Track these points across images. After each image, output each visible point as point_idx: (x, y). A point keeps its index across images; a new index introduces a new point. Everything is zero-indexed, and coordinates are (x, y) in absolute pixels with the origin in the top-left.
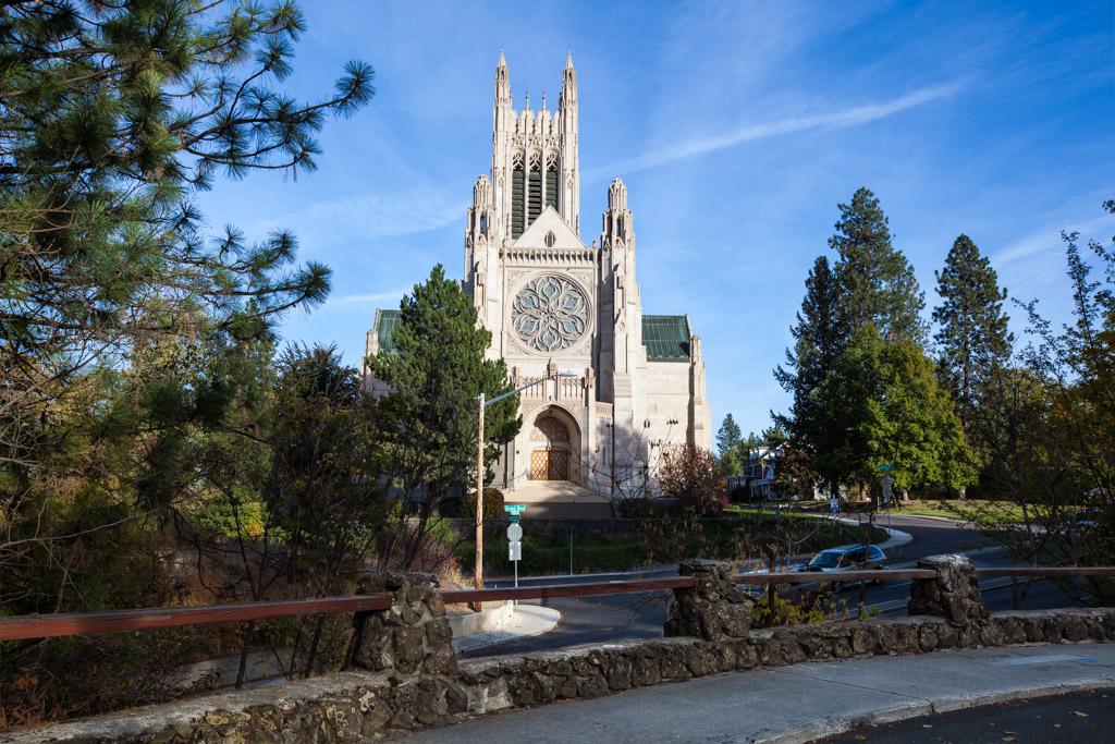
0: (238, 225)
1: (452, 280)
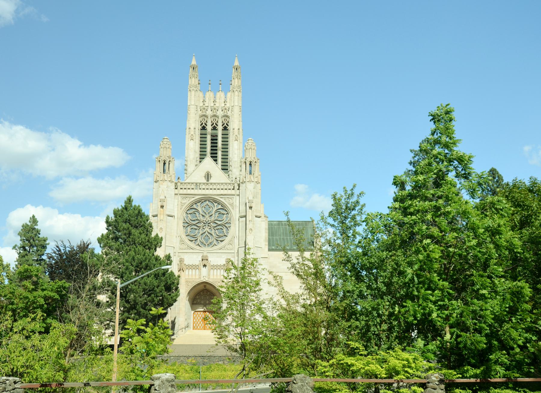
0: (455, 127)
1: (137, 205)
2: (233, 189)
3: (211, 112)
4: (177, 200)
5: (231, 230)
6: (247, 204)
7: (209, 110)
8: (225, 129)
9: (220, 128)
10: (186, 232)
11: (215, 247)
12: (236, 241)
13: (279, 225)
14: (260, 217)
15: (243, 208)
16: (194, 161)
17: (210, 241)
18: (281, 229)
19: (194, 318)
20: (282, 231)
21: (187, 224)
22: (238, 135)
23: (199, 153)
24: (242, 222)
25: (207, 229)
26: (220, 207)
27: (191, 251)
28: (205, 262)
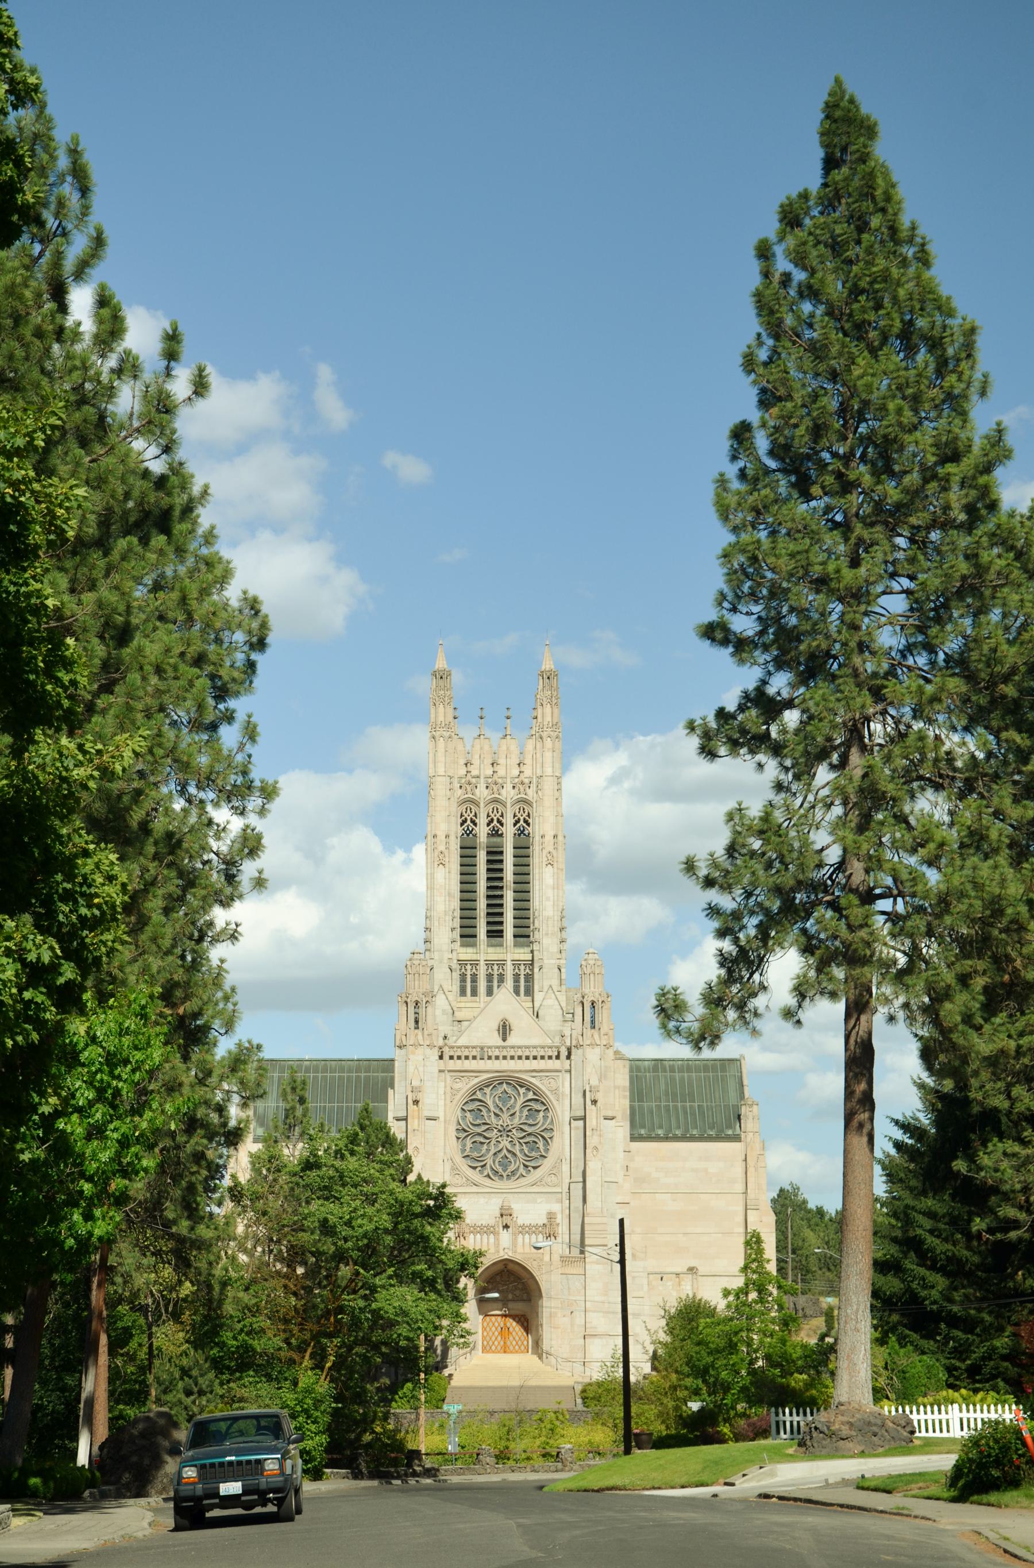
2: (558, 1057)
3: (486, 792)
4: (442, 1084)
5: (555, 1146)
6: (588, 1094)
7: (482, 786)
8: (521, 832)
9: (509, 831)
10: (463, 1150)
11: (522, 1180)
12: (565, 1168)
13: (655, 1069)
14: (612, 1118)
15: (578, 1099)
16: (449, 918)
17: (512, 1168)
18: (662, 1081)
19: (484, 1329)
20: (663, 1087)
21: (462, 1132)
22: (554, 853)
23: (457, 895)
24: (577, 1128)
25: (505, 1143)
26: (531, 1096)
27: (475, 1189)
28: (507, 1220)
